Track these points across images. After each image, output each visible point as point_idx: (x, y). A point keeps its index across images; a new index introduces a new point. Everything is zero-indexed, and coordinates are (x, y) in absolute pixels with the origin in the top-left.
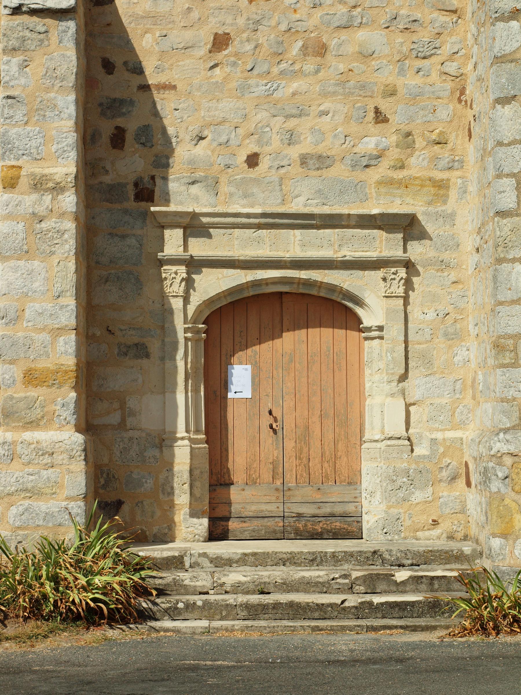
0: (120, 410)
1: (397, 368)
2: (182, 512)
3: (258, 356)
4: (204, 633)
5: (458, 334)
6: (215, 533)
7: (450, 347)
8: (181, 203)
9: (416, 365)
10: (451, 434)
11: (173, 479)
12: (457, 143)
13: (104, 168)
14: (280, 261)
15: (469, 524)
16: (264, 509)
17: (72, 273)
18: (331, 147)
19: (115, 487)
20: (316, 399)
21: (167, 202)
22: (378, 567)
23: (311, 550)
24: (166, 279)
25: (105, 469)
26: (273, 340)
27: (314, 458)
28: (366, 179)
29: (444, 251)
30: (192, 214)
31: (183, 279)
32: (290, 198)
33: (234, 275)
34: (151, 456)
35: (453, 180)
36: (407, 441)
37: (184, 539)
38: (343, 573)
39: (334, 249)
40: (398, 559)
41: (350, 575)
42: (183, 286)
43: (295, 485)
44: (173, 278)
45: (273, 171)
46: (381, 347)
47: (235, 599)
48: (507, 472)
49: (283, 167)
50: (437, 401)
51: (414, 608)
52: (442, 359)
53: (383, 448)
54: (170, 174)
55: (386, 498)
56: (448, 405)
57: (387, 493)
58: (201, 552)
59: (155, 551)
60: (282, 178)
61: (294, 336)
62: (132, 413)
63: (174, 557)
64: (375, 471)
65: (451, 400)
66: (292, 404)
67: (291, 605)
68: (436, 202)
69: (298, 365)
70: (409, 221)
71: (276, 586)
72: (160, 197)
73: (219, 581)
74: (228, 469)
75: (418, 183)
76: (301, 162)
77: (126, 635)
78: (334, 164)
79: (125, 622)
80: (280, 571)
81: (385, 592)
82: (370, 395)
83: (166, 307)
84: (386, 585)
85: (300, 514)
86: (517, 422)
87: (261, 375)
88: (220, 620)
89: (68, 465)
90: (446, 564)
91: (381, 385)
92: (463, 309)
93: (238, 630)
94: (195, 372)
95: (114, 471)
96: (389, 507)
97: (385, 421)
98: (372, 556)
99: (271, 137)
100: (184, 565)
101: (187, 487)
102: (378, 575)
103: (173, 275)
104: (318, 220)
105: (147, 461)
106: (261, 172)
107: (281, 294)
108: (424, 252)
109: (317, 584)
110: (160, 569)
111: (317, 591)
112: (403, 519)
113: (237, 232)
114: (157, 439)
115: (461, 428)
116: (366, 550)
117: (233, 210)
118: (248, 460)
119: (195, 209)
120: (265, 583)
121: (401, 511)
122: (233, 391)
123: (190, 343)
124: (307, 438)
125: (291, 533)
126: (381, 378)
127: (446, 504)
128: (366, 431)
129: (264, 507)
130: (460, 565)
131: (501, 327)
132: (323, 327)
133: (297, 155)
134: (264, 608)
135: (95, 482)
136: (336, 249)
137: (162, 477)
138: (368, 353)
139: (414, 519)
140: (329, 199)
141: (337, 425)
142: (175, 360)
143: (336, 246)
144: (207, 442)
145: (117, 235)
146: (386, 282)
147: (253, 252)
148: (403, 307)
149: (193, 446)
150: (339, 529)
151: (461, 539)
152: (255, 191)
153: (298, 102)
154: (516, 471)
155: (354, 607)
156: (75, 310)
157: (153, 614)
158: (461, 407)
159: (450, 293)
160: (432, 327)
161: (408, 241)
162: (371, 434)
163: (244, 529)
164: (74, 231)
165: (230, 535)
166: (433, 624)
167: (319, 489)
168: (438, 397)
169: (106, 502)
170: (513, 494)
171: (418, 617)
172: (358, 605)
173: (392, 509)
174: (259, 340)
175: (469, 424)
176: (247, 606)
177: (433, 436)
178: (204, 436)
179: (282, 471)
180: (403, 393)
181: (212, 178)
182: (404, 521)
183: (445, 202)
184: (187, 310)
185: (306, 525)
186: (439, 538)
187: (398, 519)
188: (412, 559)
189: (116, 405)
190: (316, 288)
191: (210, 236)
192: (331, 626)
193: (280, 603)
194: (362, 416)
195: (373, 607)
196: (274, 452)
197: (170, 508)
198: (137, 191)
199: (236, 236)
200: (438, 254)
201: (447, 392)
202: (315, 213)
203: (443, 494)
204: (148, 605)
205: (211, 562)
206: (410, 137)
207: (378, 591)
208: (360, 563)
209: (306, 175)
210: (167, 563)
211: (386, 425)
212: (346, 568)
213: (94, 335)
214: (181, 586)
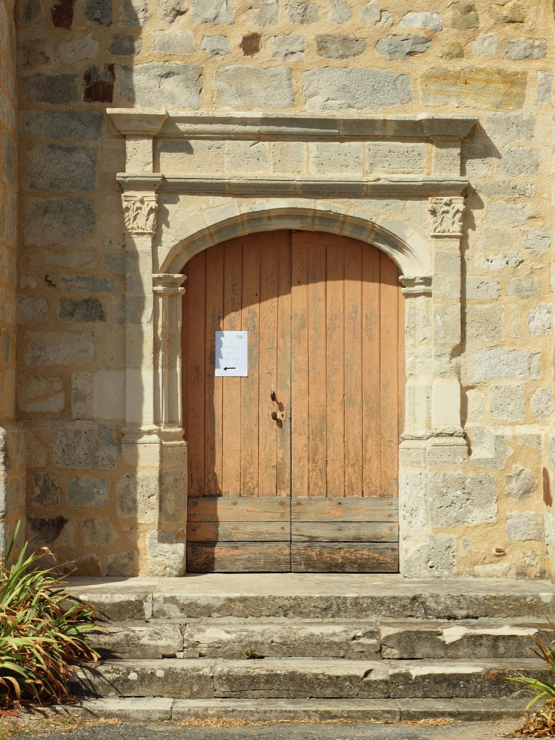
0: (63, 392)
1: (449, 337)
2: (148, 535)
3: (256, 319)
4: (163, 720)
5: (536, 289)
6: (195, 563)
7: (524, 308)
8: (150, 104)
10: (524, 430)
11: (135, 489)
12: (538, 21)
13: (43, 53)
14: (288, 186)
15: (548, 556)
18: (361, 26)
19: (55, 500)
20: (337, 379)
21: (130, 101)
22: (419, 620)
23: (324, 595)
24: (127, 209)
25: (41, 474)
26: (278, 296)
27: (333, 460)
28: (409, 71)
29: (517, 173)
30: (166, 117)
31: (151, 210)
32: (303, 98)
33: (224, 205)
34: (105, 456)
35: (531, 74)
36: (462, 439)
37: (151, 572)
38: (369, 628)
39: (364, 170)
40: (447, 608)
41: (378, 633)
42: (152, 220)
43: (307, 497)
44: (138, 209)
45: (280, 59)
46: (427, 307)
47: (212, 667)
49: (293, 53)
50: (505, 383)
51: (469, 683)
52: (513, 324)
53: (428, 449)
54: (135, 63)
55: (432, 519)
56: (520, 389)
57: (433, 511)
58: (168, 595)
59: (103, 593)
60: (291, 69)
61: (308, 291)
62: (81, 397)
63: (130, 603)
64: (417, 480)
65: (525, 381)
66: (304, 385)
67: (292, 677)
68: (506, 104)
69: (313, 332)
70: (469, 130)
72: (121, 94)
73: (190, 640)
74: (214, 475)
75: (481, 77)
76: (318, 47)
77: (48, 724)
78: (364, 50)
79: (48, 701)
80: (279, 624)
81: (429, 657)
82: (411, 374)
83: (127, 248)
84: (430, 647)
85: (314, 538)
87: (261, 345)
88: (190, 698)
90: (516, 616)
91: (428, 360)
92: (543, 255)
93: (213, 716)
94: (169, 340)
95: (54, 477)
96: (437, 531)
97: (433, 411)
98: (411, 603)
99: (277, 12)
100: (144, 615)
101: (154, 500)
102: (418, 633)
103: (138, 205)
104: (342, 128)
105: (100, 463)
106: (262, 61)
107: (290, 232)
108: (490, 175)
109: (331, 644)
110: (109, 618)
111: (330, 655)
112: (455, 547)
113: (228, 144)
114: (114, 433)
115: (538, 422)
116: (401, 595)
117: (222, 114)
118: (242, 462)
119: (170, 112)
120: (256, 643)
121: (453, 536)
122: (223, 366)
123: (161, 300)
124: (324, 433)
125: (301, 564)
126: (428, 351)
127: (516, 528)
128: (406, 424)
129: (263, 528)
130: (535, 618)
132: (348, 279)
133: (313, 37)
134: (253, 681)
135: (27, 493)
136: (367, 169)
137: (120, 485)
138: (409, 315)
139: (471, 547)
140: (357, 99)
141: (366, 416)
142: (140, 323)
143: (367, 166)
144: (185, 437)
145: (60, 148)
146: (435, 216)
148: (458, 252)
149: (164, 443)
150: (367, 559)
151: (536, 576)
152: (253, 87)
155: (383, 681)
157: (93, 688)
158: (538, 392)
159: (524, 233)
161: (467, 158)
162: (412, 429)
165: (216, 565)
166: (497, 710)
167: (340, 503)
168: (507, 377)
169: (43, 520)
171: (476, 696)
172: (389, 678)
173: (440, 534)
174: (258, 296)
175: (549, 416)
177: (499, 433)
178: (180, 429)
179: (289, 478)
180: (458, 371)
181: (193, 69)
182: (457, 550)
183: (520, 105)
184: (157, 253)
185: (321, 554)
186: (505, 574)
187: (449, 547)
188: (468, 608)
189: (58, 385)
190: (338, 225)
191: (190, 150)
192: (349, 712)
193: (277, 675)
194: (400, 403)
195: (410, 682)
196: (279, 451)
197: (131, 529)
198: (88, 86)
199: (226, 150)
200: (509, 178)
201: (520, 371)
202: (338, 118)
203: (512, 513)
204: (86, 675)
205: (182, 610)
206: (472, 13)
207: (419, 655)
208: (392, 613)
209: (325, 66)
210: (119, 611)
211: (433, 417)
212: (374, 621)
213: (27, 287)
214: (136, 646)
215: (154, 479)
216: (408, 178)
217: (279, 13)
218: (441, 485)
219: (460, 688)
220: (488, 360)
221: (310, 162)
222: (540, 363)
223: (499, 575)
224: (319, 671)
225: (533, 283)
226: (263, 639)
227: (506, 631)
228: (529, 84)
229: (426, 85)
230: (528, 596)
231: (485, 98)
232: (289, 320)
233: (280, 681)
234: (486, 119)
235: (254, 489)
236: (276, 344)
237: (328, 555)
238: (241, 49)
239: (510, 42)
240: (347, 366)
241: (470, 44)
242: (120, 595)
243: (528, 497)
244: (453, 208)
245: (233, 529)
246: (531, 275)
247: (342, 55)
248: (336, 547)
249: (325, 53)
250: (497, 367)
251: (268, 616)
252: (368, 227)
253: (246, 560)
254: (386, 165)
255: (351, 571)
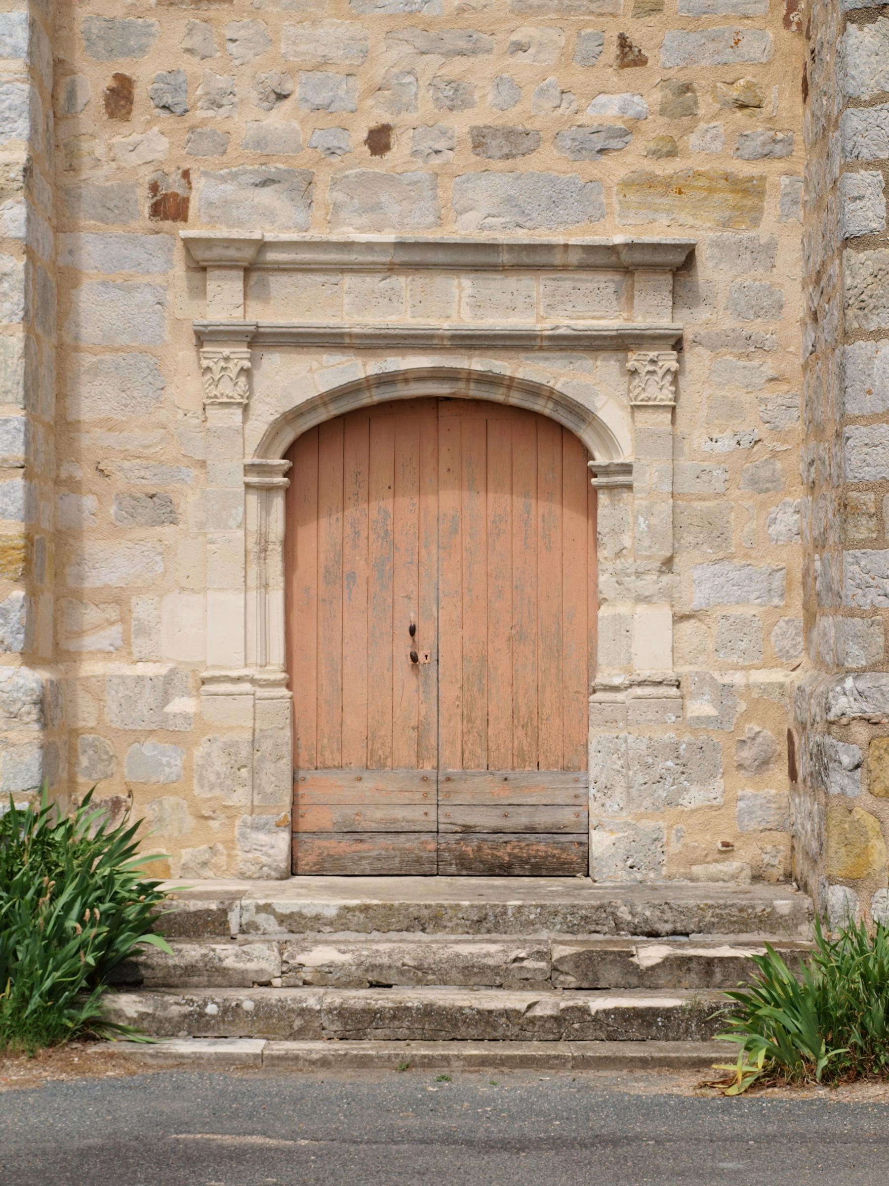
1: (657, 546)
3: (389, 522)
7: (763, 506)
9: (695, 542)
12: (782, 105)
16: (400, 817)
17: (16, 356)
18: (532, 114)
28: (601, 176)
29: (752, 317)
35: (772, 179)
38: (536, 948)
39: (538, 314)
43: (460, 770)
48: (858, 755)
49: (437, 152)
50: (736, 611)
51: (669, 1021)
52: (746, 529)
58: (262, 902)
63: (209, 912)
67: (428, 1011)
71: (402, 973)
75: (702, 184)
76: (473, 143)
78: (539, 146)
85: (470, 827)
86: (881, 657)
89: (6, 730)
90: (741, 931)
92: (789, 431)
99: (416, 94)
100: (228, 929)
109: (483, 969)
111: (482, 983)
112: (664, 840)
113: (348, 281)
114: (191, 680)
118: (370, 720)
121: (662, 824)
124: (484, 681)
125: (451, 864)
129: (399, 813)
131: (852, 467)
133: (466, 129)
136: (542, 313)
147: (378, 319)
150: (542, 857)
151: (778, 880)
152: (383, 199)
153: (469, 26)
154: (877, 753)
155: (552, 1017)
156: (23, 429)
158: (782, 623)
159: (762, 401)
160: (726, 466)
163: (360, 855)
164: (22, 276)
167: (506, 779)
168: (738, 603)
170: (869, 799)
173: (643, 821)
176: (342, 1013)
177: (726, 680)
179: (435, 744)
182: (668, 843)
183: (755, 222)
193: (408, 1009)
196: (422, 706)
199: (346, 287)
201: (756, 594)
203: (744, 792)
206: (689, 94)
209: (483, 169)
212: (545, 938)
215: (246, 744)
216: (598, 326)
217: (420, 95)
218: (646, 752)
219: (657, 1027)
220: (711, 580)
221: (463, 304)
222: (784, 583)
223: (726, 878)
224: (466, 1004)
225: (774, 471)
226: (390, 961)
227: (726, 952)
228: (768, 193)
229: (625, 196)
230: (758, 904)
231: (707, 214)
232: (436, 522)
233: (412, 1016)
234: (708, 242)
235: (386, 758)
236: (417, 557)
237: (489, 851)
238: (367, 146)
239: (742, 135)
240: (517, 587)
241: (685, 138)
242: (196, 902)
243: (768, 770)
244: (661, 368)
245: (357, 814)
246: (772, 460)
247: (507, 155)
248: (501, 840)
249: (484, 152)
250: (725, 589)
251: (398, 931)
252: (544, 393)
253: (375, 858)
254: (569, 306)
255: (521, 873)
